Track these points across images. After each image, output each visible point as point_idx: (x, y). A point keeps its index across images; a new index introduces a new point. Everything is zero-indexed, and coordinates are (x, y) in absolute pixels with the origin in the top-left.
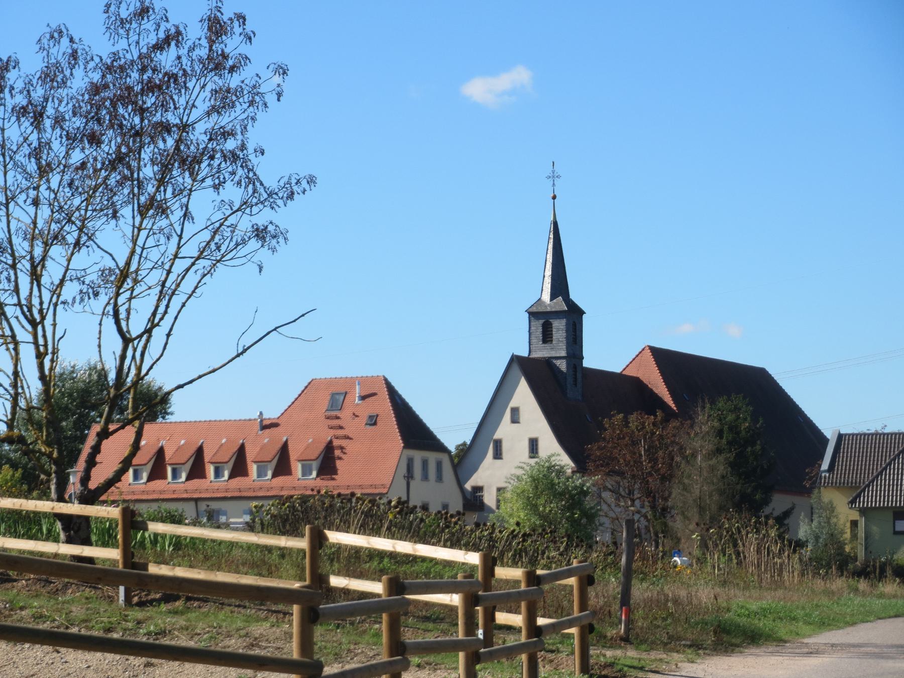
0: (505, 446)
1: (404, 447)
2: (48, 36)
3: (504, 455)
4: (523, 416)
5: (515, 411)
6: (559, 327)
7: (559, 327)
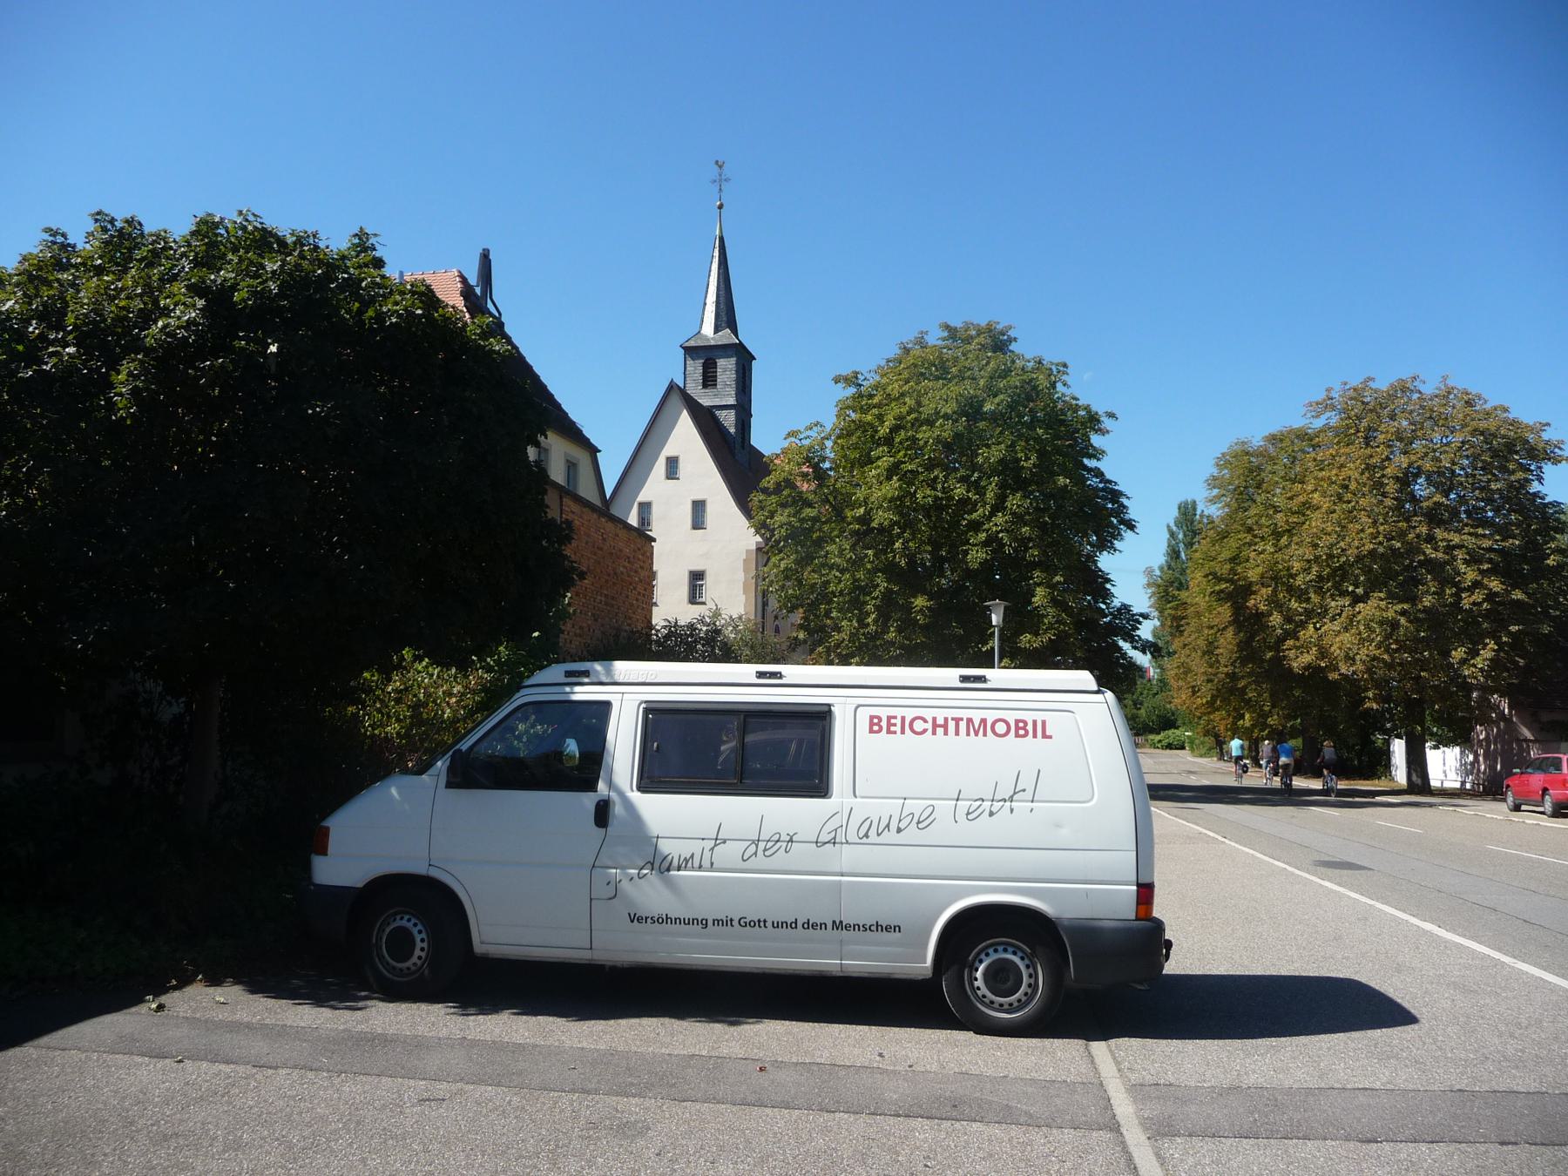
4: (684, 468)
5: (672, 463)
6: (726, 368)
7: (726, 368)
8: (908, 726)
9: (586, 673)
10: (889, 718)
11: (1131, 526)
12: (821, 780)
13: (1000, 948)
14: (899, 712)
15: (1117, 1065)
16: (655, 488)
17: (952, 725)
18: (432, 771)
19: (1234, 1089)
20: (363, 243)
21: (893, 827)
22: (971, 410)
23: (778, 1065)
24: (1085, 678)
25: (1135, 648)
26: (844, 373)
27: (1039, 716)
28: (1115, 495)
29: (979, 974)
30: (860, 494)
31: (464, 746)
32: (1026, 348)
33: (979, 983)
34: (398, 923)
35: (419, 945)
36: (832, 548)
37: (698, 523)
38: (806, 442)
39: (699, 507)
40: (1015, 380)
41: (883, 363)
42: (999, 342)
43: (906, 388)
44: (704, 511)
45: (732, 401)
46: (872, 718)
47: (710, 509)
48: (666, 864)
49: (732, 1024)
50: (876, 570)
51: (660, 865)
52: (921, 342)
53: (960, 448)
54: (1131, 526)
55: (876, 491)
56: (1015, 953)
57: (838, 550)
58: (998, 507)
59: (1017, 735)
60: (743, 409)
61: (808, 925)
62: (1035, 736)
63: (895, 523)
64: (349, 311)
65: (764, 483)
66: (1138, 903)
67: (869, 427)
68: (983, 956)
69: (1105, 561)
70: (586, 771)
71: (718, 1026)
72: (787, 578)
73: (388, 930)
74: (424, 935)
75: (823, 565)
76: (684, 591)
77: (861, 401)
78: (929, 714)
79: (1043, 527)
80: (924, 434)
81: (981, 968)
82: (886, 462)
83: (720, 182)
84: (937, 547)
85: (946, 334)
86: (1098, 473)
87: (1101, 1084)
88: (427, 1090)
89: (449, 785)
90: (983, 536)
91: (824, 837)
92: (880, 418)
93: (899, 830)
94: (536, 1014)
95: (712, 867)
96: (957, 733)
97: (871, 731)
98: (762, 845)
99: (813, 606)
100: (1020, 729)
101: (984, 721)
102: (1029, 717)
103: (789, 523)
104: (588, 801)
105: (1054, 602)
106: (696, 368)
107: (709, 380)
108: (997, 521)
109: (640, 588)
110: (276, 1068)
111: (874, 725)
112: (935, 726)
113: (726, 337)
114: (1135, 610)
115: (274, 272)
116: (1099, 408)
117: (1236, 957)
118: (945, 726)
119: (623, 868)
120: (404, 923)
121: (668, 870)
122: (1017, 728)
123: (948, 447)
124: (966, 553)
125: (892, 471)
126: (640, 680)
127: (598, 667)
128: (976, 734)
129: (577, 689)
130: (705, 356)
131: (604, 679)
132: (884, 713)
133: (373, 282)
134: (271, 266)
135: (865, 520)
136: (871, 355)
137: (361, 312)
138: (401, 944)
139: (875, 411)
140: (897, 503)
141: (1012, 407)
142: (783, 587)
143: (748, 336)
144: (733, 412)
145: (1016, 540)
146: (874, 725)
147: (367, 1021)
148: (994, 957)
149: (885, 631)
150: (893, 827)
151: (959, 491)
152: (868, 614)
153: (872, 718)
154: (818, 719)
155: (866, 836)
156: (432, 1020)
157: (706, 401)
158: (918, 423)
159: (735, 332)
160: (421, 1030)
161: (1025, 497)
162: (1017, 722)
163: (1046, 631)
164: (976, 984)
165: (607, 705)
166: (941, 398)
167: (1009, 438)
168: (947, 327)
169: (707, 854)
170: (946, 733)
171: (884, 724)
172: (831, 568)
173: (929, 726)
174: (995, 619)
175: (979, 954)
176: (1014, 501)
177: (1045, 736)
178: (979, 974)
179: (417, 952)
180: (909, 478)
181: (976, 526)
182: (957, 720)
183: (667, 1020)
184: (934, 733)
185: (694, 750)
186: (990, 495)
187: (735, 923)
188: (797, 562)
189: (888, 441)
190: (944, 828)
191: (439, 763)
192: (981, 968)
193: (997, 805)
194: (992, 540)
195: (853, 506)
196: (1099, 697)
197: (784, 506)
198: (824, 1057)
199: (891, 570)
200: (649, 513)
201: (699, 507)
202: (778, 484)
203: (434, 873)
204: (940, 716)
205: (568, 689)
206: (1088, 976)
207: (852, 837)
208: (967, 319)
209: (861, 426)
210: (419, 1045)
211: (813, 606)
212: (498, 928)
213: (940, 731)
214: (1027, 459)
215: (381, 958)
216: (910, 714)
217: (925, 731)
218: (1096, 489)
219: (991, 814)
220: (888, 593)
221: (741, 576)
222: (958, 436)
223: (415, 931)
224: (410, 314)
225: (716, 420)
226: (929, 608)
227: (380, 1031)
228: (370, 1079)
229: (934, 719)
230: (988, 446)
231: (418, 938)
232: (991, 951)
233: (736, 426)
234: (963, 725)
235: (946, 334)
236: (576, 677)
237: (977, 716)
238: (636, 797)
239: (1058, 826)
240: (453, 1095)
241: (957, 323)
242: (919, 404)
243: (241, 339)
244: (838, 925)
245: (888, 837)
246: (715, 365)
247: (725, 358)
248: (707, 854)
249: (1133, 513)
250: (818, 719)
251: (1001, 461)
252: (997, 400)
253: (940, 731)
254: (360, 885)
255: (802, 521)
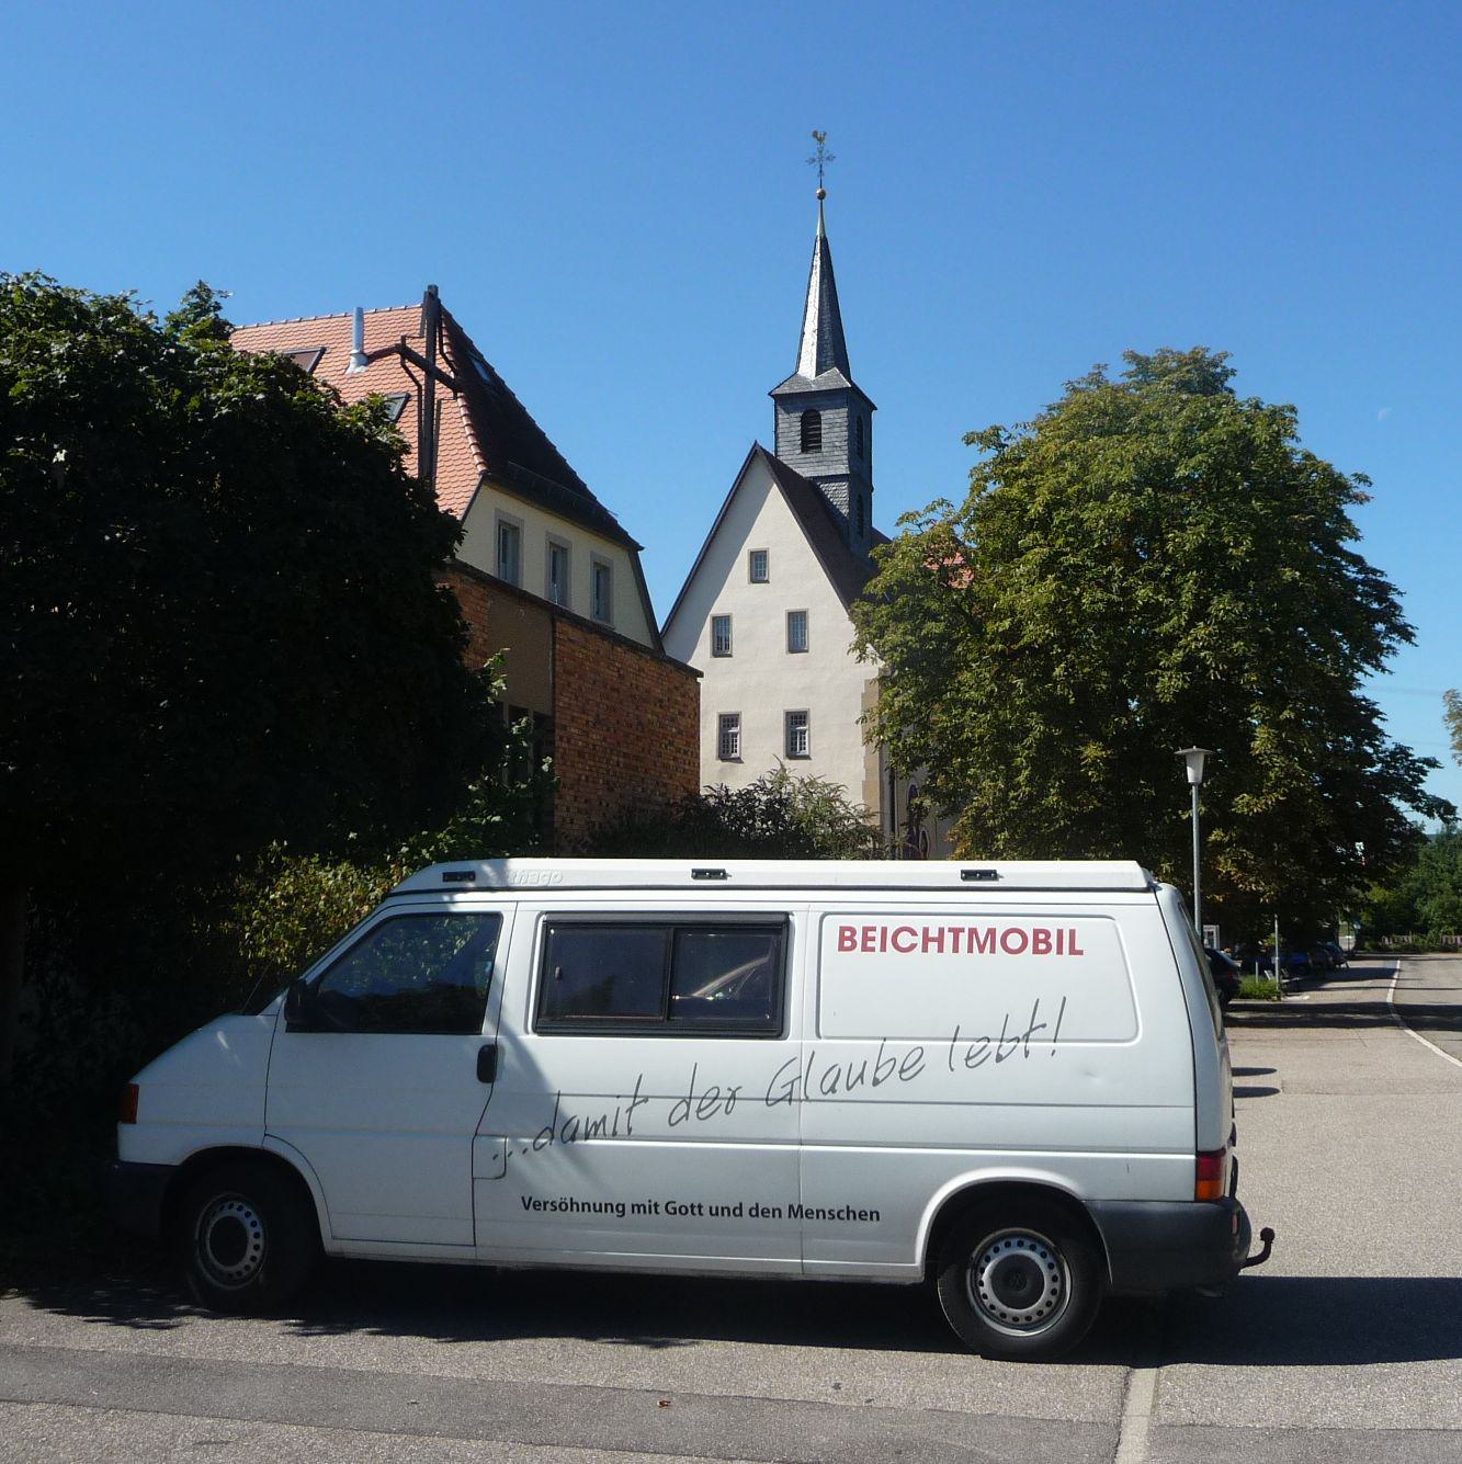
0: (737, 629)
1: (486, 478)
2: (56, 285)
3: (735, 647)
4: (775, 568)
5: (759, 561)
6: (834, 423)
7: (834, 423)
8: (891, 940)
9: (471, 876)
10: (866, 930)
11: (1406, 634)
12: (774, 1017)
13: (1014, 1241)
14: (878, 922)
15: (1152, 1397)
16: (735, 595)
17: (949, 938)
18: (270, 1009)
19: (1296, 1431)
20: (203, 301)
21: (869, 1077)
22: (1157, 475)
23: (690, 1398)
24: (1129, 871)
25: (1418, 809)
26: (978, 431)
27: (1066, 925)
28: (1382, 590)
29: (985, 1277)
30: (1004, 600)
31: (310, 976)
32: (1247, 386)
33: (986, 1289)
34: (227, 1213)
35: (252, 1241)
36: (965, 676)
37: (797, 644)
38: (926, 528)
39: (797, 621)
40: (1220, 432)
41: (1044, 412)
42: (1206, 378)
43: (1066, 448)
44: (804, 626)
45: (843, 469)
46: (843, 930)
48: (569, 1132)
49: (658, 1346)
50: (1030, 707)
51: (563, 1132)
52: (1097, 379)
53: (1145, 528)
54: (1406, 634)
55: (1028, 594)
56: (1033, 1248)
57: (974, 680)
58: (1199, 613)
59: (1036, 951)
60: (860, 480)
61: (756, 1211)
62: (1060, 951)
63: (1054, 640)
64: (166, 401)
65: (869, 588)
66: (1197, 1179)
67: (1020, 502)
68: (991, 1252)
69: (1371, 686)
70: (457, 1002)
71: (637, 1349)
72: (905, 721)
73: (213, 1223)
74: (259, 1229)
75: (954, 701)
77: (1008, 466)
78: (918, 923)
79: (1264, 641)
80: (1091, 514)
81: (988, 1269)
82: (1036, 555)
83: (821, 161)
84: (1117, 671)
85: (1133, 367)
86: (1357, 560)
87: (1118, 1425)
88: (213, 1429)
89: (291, 1028)
90: (1178, 656)
91: (777, 1093)
92: (1031, 491)
93: (876, 1082)
94: (398, 1334)
95: (630, 1135)
96: (956, 949)
97: (842, 948)
98: (695, 1104)
99: (942, 761)
100: (1041, 942)
101: (991, 932)
102: (1051, 925)
103: (905, 644)
104: (469, 1046)
105: (1284, 748)
106: (792, 424)
107: (810, 440)
108: (1197, 635)
109: (679, 743)
110: (28, 1403)
111: (846, 939)
112: (926, 939)
113: (833, 379)
114: (1417, 754)
115: (60, 356)
116: (1344, 468)
117: (1409, 1254)
118: (940, 940)
119: (514, 1137)
120: (234, 1212)
121: (573, 1138)
122: (1036, 941)
123: (1129, 528)
124: (1154, 680)
125: (1048, 565)
126: (541, 884)
127: (486, 868)
128: (981, 950)
129: (459, 897)
130: (803, 406)
131: (494, 884)
132: (858, 923)
133: (209, 359)
134: (57, 349)
135: (1013, 634)
136: (1023, 403)
137: (182, 401)
138: (230, 1240)
139: (1022, 482)
140: (1053, 611)
141: (1217, 469)
142: (898, 735)
143: (865, 377)
144: (845, 486)
145: (1225, 660)
146: (846, 939)
147: (172, 1342)
148: (1005, 1253)
149: (1043, 793)
150: (869, 1077)
151: (1143, 593)
152: (1018, 771)
153: (843, 930)
154: (771, 933)
155: (833, 1090)
156: (264, 1343)
157: (806, 472)
158: (1084, 498)
159: (846, 372)
160: (240, 1354)
161: (1237, 598)
162: (1037, 932)
163: (1275, 788)
164: (983, 1290)
165: (496, 918)
166: (1115, 460)
167: (1210, 513)
168: (1134, 357)
169: (623, 1116)
170: (941, 950)
171: (859, 938)
172: (966, 704)
173: (919, 940)
174: (1192, 774)
175: (986, 1248)
176: (1221, 605)
177: (1073, 951)
178: (985, 1277)
179: (250, 1252)
180: (1071, 576)
181: (1170, 642)
182: (956, 932)
183: (570, 1342)
184: (925, 949)
185: (610, 977)
186: (1186, 597)
187: (661, 1209)
188: (918, 698)
189: (1043, 524)
190: (936, 1079)
191: (279, 999)
192: (988, 1269)
193: (1007, 1046)
194: (1190, 662)
195: (999, 615)
196: (1150, 897)
197: (898, 619)
198: (757, 1388)
199: (1051, 708)
200: (728, 631)
201: (797, 621)
202: (889, 589)
203: (272, 1146)
204: (933, 926)
205: (446, 898)
206: (1150, 1277)
207: (814, 1092)
208: (1164, 346)
209: (1001, 502)
210: (228, 1372)
211: (942, 761)
212: (360, 1214)
213: (933, 946)
214: (1238, 544)
215: (205, 1259)
216: (893, 924)
217: (913, 946)
218: (1355, 582)
219: (999, 1058)
220: (1046, 743)
222: (1138, 513)
223: (247, 1222)
224: (247, 400)
225: (821, 496)
226: (1106, 761)
227: (184, 1355)
228: (144, 1416)
229: (926, 931)
230: (1183, 528)
231: (251, 1232)
232: (1001, 1245)
234: (964, 938)
235: (1133, 367)
236: (459, 881)
237: (982, 926)
238: (531, 1040)
239: (1089, 1074)
240: (243, 1435)
241: (1149, 351)
242: (1084, 468)
243: (18, 445)
244: (796, 1211)
245: (862, 1091)
247: (834, 408)
248: (623, 1116)
249: (1409, 616)
250: (771, 933)
251: (1202, 548)
252: (1192, 462)
253: (933, 946)
254: (177, 1163)
255: (924, 640)
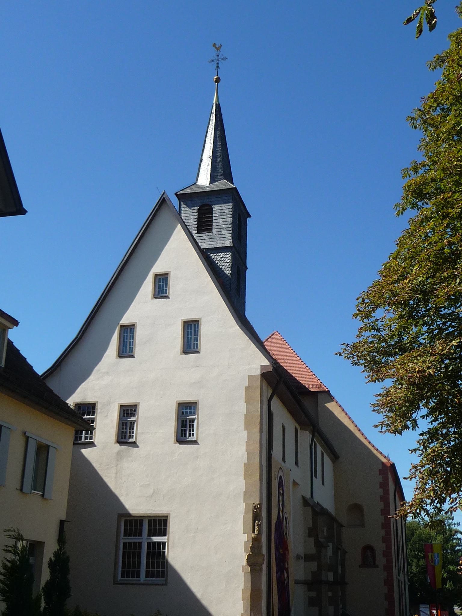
6: (222, 214)
7: (222, 214)
39: (191, 329)
45: (228, 243)
47: (204, 330)
76: (170, 427)
83: (218, 61)
113: (222, 184)
165: (164, 544)
201: (191, 329)
221: (241, 407)
233: (232, 268)
246: (211, 211)
